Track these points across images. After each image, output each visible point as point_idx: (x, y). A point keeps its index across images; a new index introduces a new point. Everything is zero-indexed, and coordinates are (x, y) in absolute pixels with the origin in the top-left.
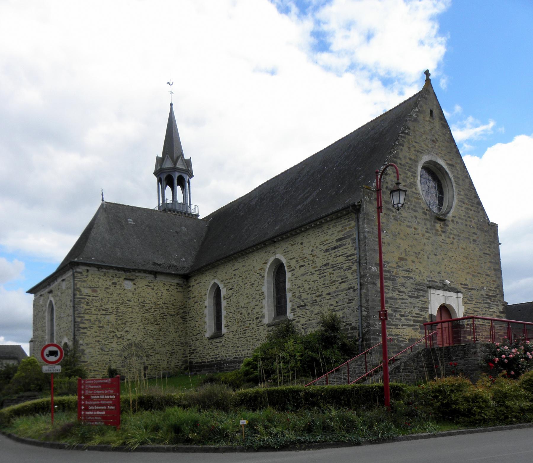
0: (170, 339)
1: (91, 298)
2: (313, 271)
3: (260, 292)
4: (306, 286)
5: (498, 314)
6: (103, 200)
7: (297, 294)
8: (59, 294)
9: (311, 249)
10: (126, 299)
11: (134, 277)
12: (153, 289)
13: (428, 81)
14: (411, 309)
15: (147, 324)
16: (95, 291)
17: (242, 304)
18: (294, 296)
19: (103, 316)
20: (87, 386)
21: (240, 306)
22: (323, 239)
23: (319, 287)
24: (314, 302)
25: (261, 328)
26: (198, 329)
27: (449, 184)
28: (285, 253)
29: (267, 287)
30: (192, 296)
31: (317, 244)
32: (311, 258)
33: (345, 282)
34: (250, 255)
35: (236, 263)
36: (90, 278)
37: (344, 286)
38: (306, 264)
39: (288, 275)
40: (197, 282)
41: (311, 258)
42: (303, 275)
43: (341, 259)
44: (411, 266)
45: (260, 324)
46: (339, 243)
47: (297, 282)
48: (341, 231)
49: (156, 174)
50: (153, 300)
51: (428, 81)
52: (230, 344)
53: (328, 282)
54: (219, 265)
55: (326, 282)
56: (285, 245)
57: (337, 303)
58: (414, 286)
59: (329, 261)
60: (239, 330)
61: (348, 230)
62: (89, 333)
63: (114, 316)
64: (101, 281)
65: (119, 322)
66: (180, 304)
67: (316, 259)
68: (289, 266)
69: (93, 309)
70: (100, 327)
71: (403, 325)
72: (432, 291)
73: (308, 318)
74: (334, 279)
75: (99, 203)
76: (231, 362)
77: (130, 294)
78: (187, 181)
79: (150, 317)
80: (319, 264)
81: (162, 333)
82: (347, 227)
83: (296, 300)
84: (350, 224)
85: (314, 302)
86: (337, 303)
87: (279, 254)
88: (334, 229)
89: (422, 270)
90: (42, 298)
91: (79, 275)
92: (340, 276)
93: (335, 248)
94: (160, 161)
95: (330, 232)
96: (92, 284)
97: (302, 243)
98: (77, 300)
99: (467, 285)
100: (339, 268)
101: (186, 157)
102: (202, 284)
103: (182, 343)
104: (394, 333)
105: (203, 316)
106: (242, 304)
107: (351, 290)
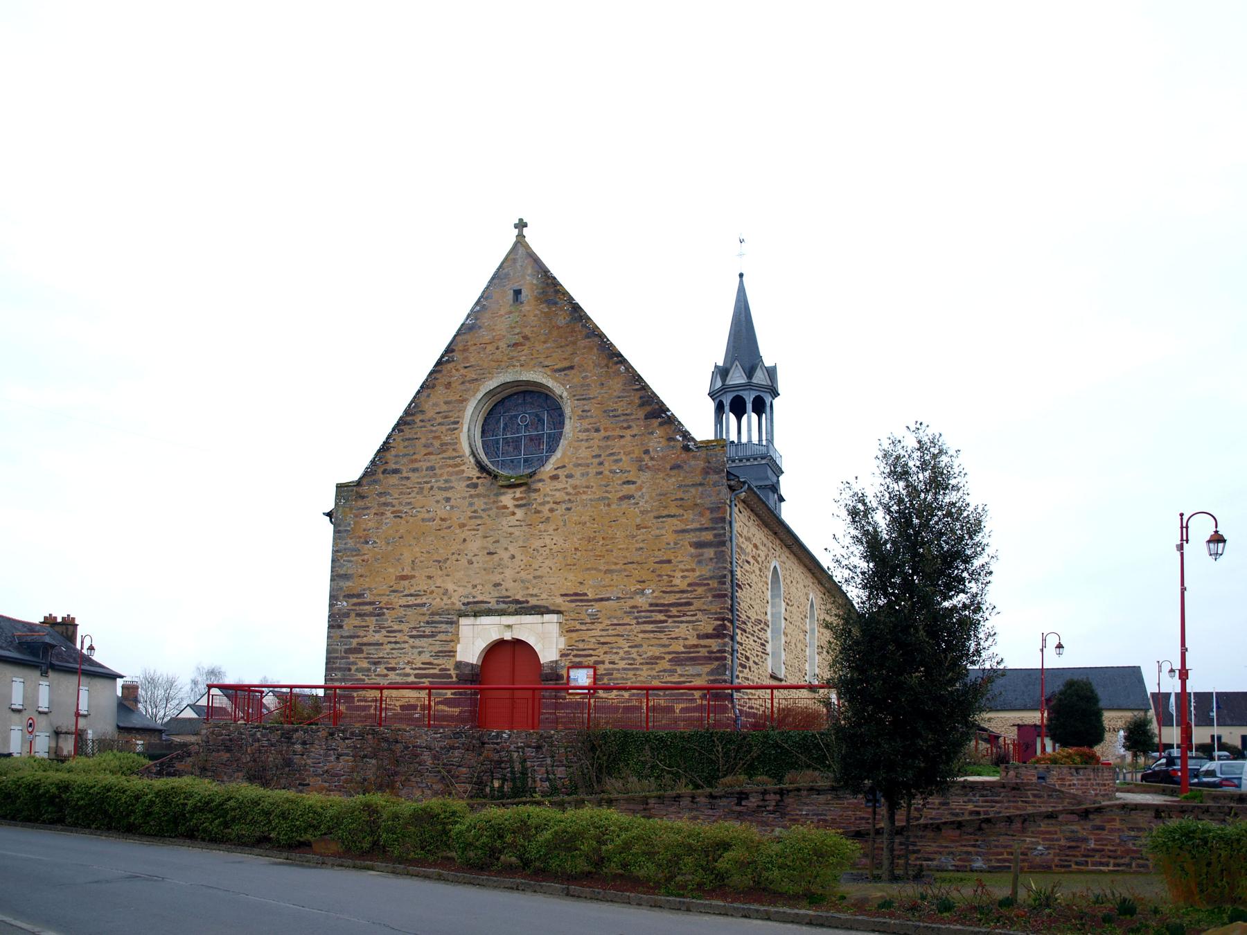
13: (741, 282)
72: (463, 621)
78: (768, 404)
94: (722, 372)
99: (586, 594)
101: (768, 363)
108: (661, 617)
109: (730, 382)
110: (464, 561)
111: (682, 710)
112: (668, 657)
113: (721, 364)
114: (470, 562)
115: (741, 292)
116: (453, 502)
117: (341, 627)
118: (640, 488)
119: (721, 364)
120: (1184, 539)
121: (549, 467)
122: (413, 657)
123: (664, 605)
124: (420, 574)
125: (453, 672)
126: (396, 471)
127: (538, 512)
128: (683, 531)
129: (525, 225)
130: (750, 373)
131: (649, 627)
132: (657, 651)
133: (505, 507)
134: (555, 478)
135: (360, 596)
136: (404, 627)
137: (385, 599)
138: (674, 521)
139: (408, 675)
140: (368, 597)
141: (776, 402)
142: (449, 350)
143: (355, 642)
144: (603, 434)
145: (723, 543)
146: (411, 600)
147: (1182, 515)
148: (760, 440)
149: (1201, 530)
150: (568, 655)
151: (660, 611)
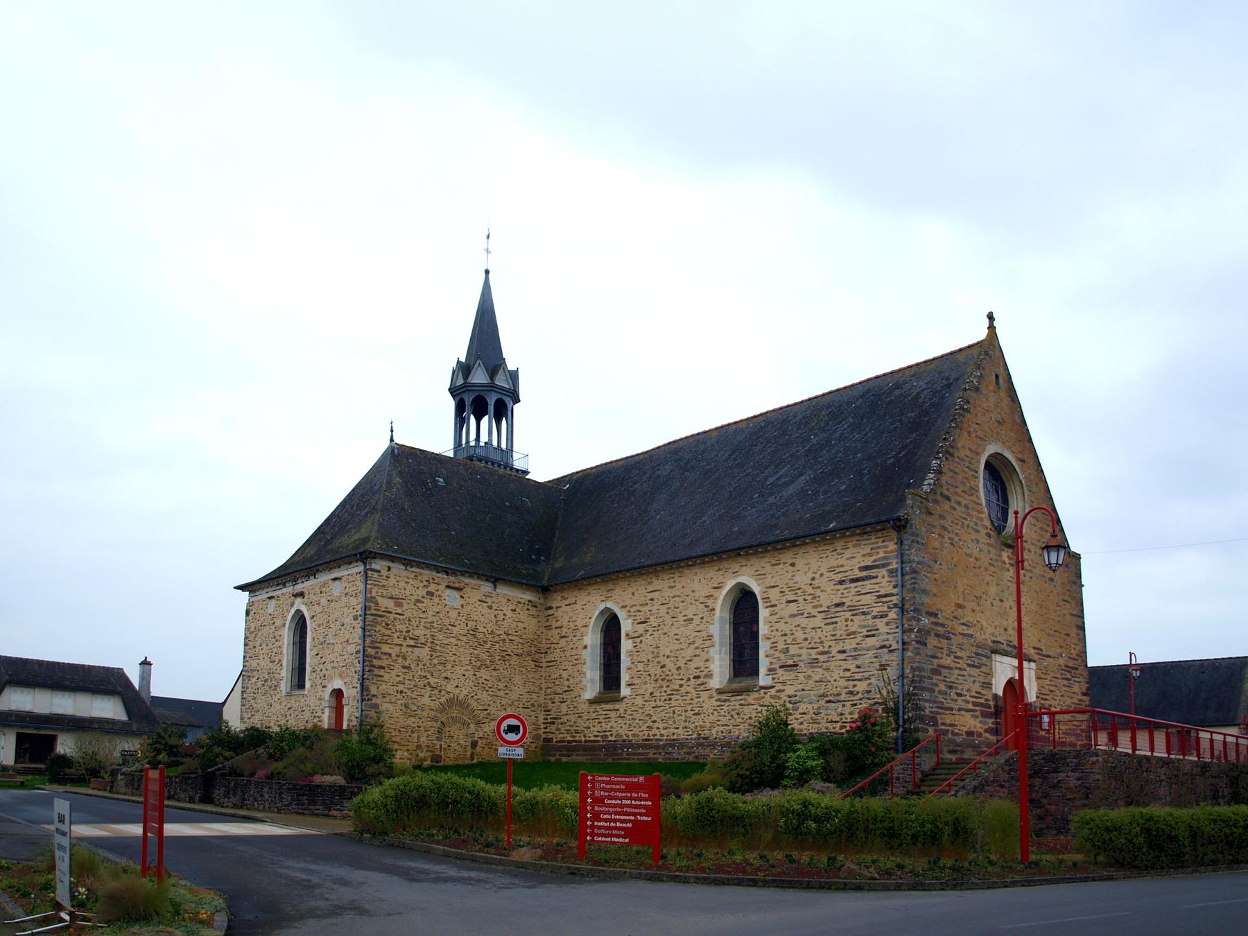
0: (514, 696)
1: (392, 616)
2: (814, 612)
3: (703, 634)
4: (800, 635)
5: (1080, 697)
6: (392, 440)
7: (781, 646)
8: (324, 601)
9: (810, 575)
10: (447, 622)
11: (461, 585)
12: (490, 607)
13: (992, 328)
14: (969, 684)
15: (479, 668)
16: (400, 605)
17: (665, 651)
18: (774, 648)
19: (410, 649)
20: (597, 785)
21: (661, 654)
22: (834, 563)
23: (823, 638)
24: (814, 663)
25: (704, 695)
26: (566, 683)
27: (1018, 489)
28: (759, 576)
29: (719, 627)
30: (554, 624)
31: (823, 570)
32: (811, 591)
33: (873, 636)
34: (686, 571)
35: (654, 580)
36: (392, 581)
37: (871, 642)
38: (801, 599)
39: (763, 613)
40: (567, 602)
41: (811, 591)
42: (792, 616)
43: (867, 599)
44: (969, 618)
45: (702, 688)
46: (864, 574)
47: (781, 625)
48: (870, 555)
49: (453, 391)
50: (490, 627)
51: (992, 328)
52: (637, 716)
53: (842, 632)
54: (618, 578)
55: (838, 633)
56: (762, 564)
57: (858, 667)
58: (974, 649)
59: (844, 600)
60: (657, 694)
61: (882, 555)
62: (387, 677)
63: (427, 649)
64: (409, 587)
65: (435, 661)
66: (531, 636)
67: (818, 592)
68: (766, 599)
69: (395, 635)
70: (404, 667)
71: (960, 710)
72: (997, 657)
73: (801, 687)
74: (853, 629)
75: (386, 444)
76: (639, 746)
77: (453, 614)
79: (484, 656)
80: (825, 601)
81: (501, 685)
82: (881, 551)
83: (777, 654)
84: (886, 547)
85: (814, 663)
86: (858, 667)
87: (747, 576)
88: (855, 550)
89: (985, 624)
90: (273, 602)
91: (376, 575)
92: (864, 626)
93: (857, 580)
94: (464, 369)
95: (848, 553)
96: (395, 592)
97: (793, 565)
98: (370, 618)
100: (864, 613)
102: (578, 606)
103: (533, 705)
104: (948, 722)
105: (578, 662)
106: (665, 651)
107: (886, 650)
113: (463, 359)
119: (463, 359)
125: (992, 703)
130: (493, 372)
141: (516, 407)
148: (468, 442)
150: (706, 676)
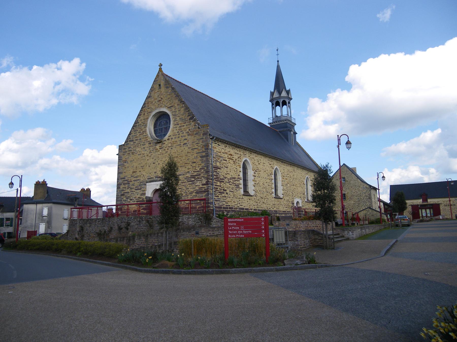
13: (278, 63)
72: (147, 184)
108: (193, 179)
109: (274, 96)
110: (148, 166)
111: (199, 208)
112: (195, 191)
114: (149, 166)
115: (278, 67)
116: (145, 149)
117: (120, 188)
118: (188, 141)
120: (339, 144)
121: (166, 137)
122: (136, 195)
123: (194, 176)
124: (138, 171)
126: (133, 141)
127: (165, 150)
128: (198, 153)
129: (162, 65)
131: (190, 183)
132: (192, 190)
133: (157, 149)
134: (168, 139)
135: (124, 178)
136: (134, 187)
137: (130, 179)
138: (196, 150)
139: (135, 201)
140: (126, 179)
142: (144, 104)
143: (123, 192)
144: (180, 125)
145: (208, 156)
146: (136, 179)
147: (338, 136)
149: (344, 140)
151: (193, 178)
